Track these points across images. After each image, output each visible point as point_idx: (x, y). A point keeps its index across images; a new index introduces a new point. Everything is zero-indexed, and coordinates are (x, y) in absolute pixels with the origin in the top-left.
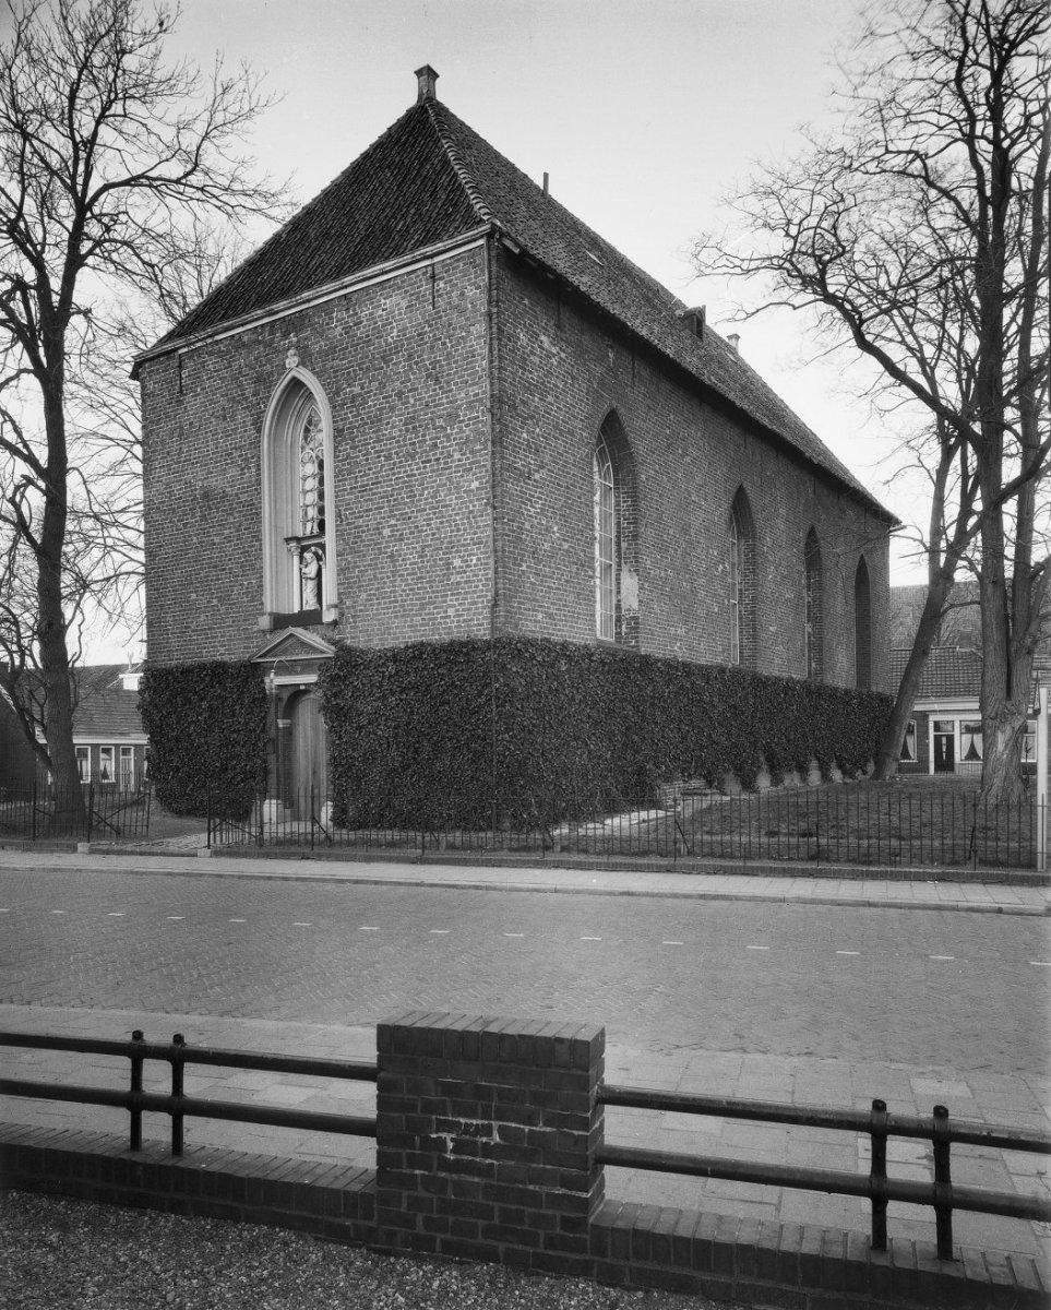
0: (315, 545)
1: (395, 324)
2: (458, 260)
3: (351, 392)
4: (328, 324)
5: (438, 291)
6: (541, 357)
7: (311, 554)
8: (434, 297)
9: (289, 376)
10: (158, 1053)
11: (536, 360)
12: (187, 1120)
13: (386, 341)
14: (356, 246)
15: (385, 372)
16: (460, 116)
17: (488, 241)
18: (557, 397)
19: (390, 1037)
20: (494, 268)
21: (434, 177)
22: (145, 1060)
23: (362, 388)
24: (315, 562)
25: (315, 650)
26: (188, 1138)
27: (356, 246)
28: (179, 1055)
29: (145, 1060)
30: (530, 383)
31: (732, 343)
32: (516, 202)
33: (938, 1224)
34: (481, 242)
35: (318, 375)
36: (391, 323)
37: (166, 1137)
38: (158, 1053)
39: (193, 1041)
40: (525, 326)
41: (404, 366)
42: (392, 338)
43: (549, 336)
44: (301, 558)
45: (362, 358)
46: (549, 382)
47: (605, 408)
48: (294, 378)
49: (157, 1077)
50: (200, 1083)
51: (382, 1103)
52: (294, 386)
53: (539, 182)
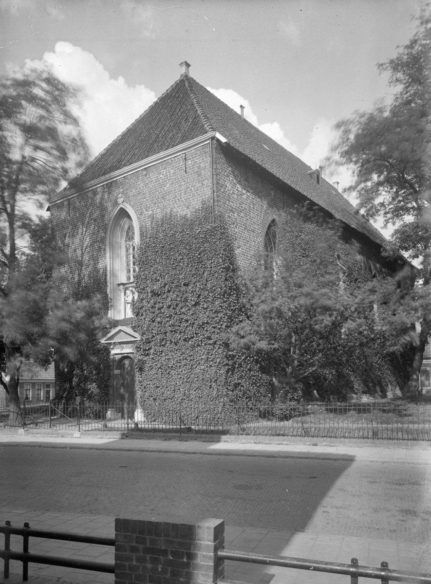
0: (131, 287)
1: (168, 181)
2: (197, 151)
3: (148, 214)
4: (137, 182)
5: (188, 165)
6: (238, 195)
7: (129, 291)
8: (186, 168)
9: (119, 208)
10: (17, 532)
11: (235, 196)
12: (30, 564)
13: (163, 189)
14: (150, 146)
15: (164, 204)
16: (201, 84)
17: (212, 141)
18: (246, 214)
19: (120, 524)
20: (214, 154)
21: (187, 112)
22: (29, 537)
23: (153, 212)
24: (131, 295)
25: (135, 338)
26: (30, 573)
27: (150, 146)
28: (27, 533)
29: (29, 537)
30: (233, 208)
31: (335, 186)
32: (226, 122)
33: (5, 572)
34: (208, 142)
35: (133, 206)
36: (166, 181)
37: (21, 571)
38: (17, 532)
39: (34, 527)
40: (229, 180)
41: (172, 201)
42: (167, 188)
43: (241, 185)
44: (125, 293)
45: (152, 198)
46: (241, 207)
47: (270, 219)
48: (121, 208)
49: (17, 544)
50: (38, 547)
51: (117, 558)
52: (122, 211)
53: (239, 111)
